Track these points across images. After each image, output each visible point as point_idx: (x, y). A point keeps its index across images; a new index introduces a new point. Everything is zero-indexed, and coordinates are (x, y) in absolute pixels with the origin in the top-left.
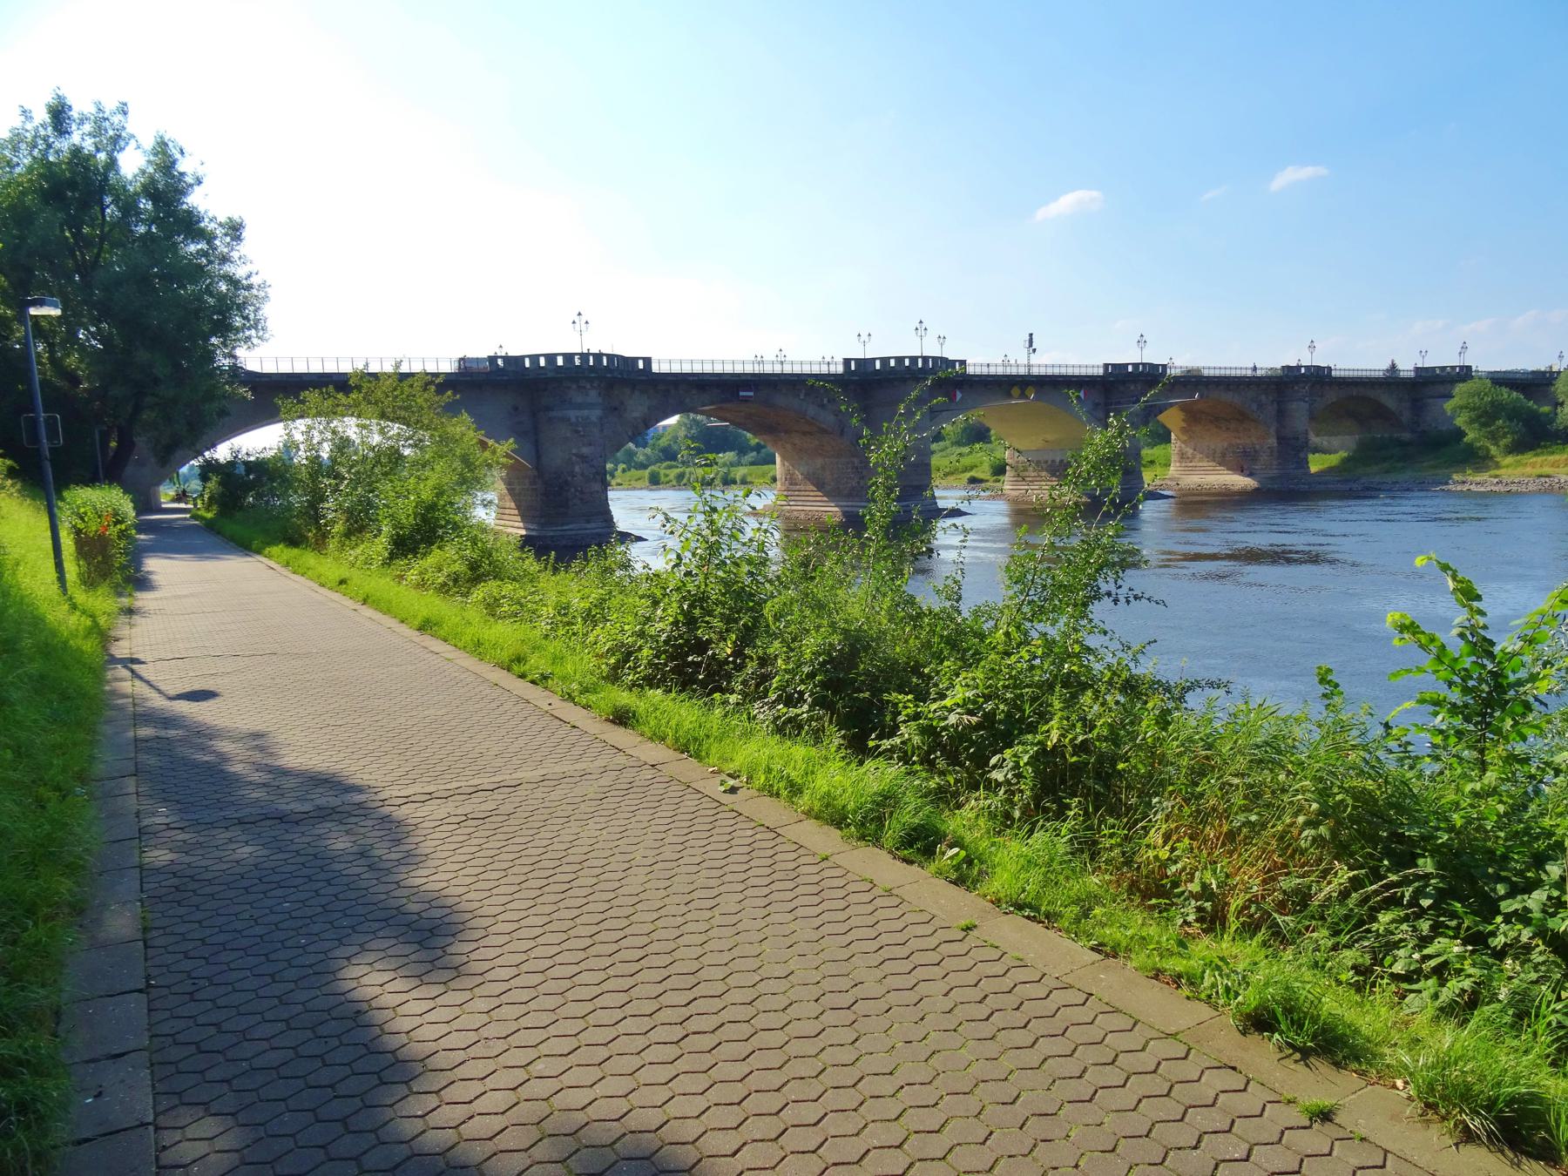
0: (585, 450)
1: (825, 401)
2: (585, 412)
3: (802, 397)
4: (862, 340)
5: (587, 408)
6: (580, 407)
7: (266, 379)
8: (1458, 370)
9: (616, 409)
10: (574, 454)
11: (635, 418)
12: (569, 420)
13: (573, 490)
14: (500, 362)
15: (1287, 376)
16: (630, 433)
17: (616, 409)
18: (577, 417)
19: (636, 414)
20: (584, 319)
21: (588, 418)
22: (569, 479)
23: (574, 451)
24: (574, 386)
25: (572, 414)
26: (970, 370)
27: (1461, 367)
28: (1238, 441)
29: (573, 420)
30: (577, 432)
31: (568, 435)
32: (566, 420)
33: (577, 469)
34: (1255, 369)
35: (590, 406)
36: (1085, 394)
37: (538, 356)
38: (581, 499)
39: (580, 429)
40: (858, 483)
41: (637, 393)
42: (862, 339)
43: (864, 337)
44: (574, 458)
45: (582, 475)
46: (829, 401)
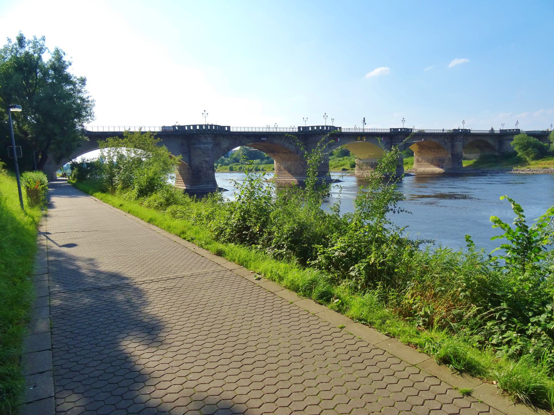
0: (207, 159)
1: (292, 141)
2: (207, 146)
3: (283, 140)
4: (304, 120)
5: (208, 144)
6: (205, 144)
7: (246, 133)
8: (515, 130)
9: (218, 144)
10: (203, 160)
11: (224, 148)
12: (201, 148)
13: (202, 173)
14: (177, 128)
15: (455, 133)
16: (223, 153)
17: (218, 144)
18: (204, 147)
19: (225, 146)
20: (206, 113)
21: (208, 147)
22: (201, 169)
23: (203, 159)
24: (203, 136)
25: (202, 146)
26: (343, 131)
27: (516, 130)
28: (438, 156)
29: (203, 148)
30: (204, 152)
31: (201, 153)
32: (200, 148)
33: (204, 165)
34: (443, 130)
35: (209, 143)
36: (383, 139)
37: (190, 126)
38: (205, 176)
39: (205, 151)
40: (303, 170)
41: (225, 139)
42: (305, 120)
43: (305, 119)
44: (203, 162)
45: (206, 167)
46: (293, 142)
